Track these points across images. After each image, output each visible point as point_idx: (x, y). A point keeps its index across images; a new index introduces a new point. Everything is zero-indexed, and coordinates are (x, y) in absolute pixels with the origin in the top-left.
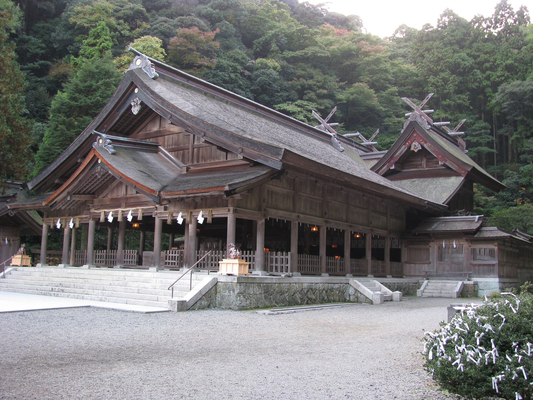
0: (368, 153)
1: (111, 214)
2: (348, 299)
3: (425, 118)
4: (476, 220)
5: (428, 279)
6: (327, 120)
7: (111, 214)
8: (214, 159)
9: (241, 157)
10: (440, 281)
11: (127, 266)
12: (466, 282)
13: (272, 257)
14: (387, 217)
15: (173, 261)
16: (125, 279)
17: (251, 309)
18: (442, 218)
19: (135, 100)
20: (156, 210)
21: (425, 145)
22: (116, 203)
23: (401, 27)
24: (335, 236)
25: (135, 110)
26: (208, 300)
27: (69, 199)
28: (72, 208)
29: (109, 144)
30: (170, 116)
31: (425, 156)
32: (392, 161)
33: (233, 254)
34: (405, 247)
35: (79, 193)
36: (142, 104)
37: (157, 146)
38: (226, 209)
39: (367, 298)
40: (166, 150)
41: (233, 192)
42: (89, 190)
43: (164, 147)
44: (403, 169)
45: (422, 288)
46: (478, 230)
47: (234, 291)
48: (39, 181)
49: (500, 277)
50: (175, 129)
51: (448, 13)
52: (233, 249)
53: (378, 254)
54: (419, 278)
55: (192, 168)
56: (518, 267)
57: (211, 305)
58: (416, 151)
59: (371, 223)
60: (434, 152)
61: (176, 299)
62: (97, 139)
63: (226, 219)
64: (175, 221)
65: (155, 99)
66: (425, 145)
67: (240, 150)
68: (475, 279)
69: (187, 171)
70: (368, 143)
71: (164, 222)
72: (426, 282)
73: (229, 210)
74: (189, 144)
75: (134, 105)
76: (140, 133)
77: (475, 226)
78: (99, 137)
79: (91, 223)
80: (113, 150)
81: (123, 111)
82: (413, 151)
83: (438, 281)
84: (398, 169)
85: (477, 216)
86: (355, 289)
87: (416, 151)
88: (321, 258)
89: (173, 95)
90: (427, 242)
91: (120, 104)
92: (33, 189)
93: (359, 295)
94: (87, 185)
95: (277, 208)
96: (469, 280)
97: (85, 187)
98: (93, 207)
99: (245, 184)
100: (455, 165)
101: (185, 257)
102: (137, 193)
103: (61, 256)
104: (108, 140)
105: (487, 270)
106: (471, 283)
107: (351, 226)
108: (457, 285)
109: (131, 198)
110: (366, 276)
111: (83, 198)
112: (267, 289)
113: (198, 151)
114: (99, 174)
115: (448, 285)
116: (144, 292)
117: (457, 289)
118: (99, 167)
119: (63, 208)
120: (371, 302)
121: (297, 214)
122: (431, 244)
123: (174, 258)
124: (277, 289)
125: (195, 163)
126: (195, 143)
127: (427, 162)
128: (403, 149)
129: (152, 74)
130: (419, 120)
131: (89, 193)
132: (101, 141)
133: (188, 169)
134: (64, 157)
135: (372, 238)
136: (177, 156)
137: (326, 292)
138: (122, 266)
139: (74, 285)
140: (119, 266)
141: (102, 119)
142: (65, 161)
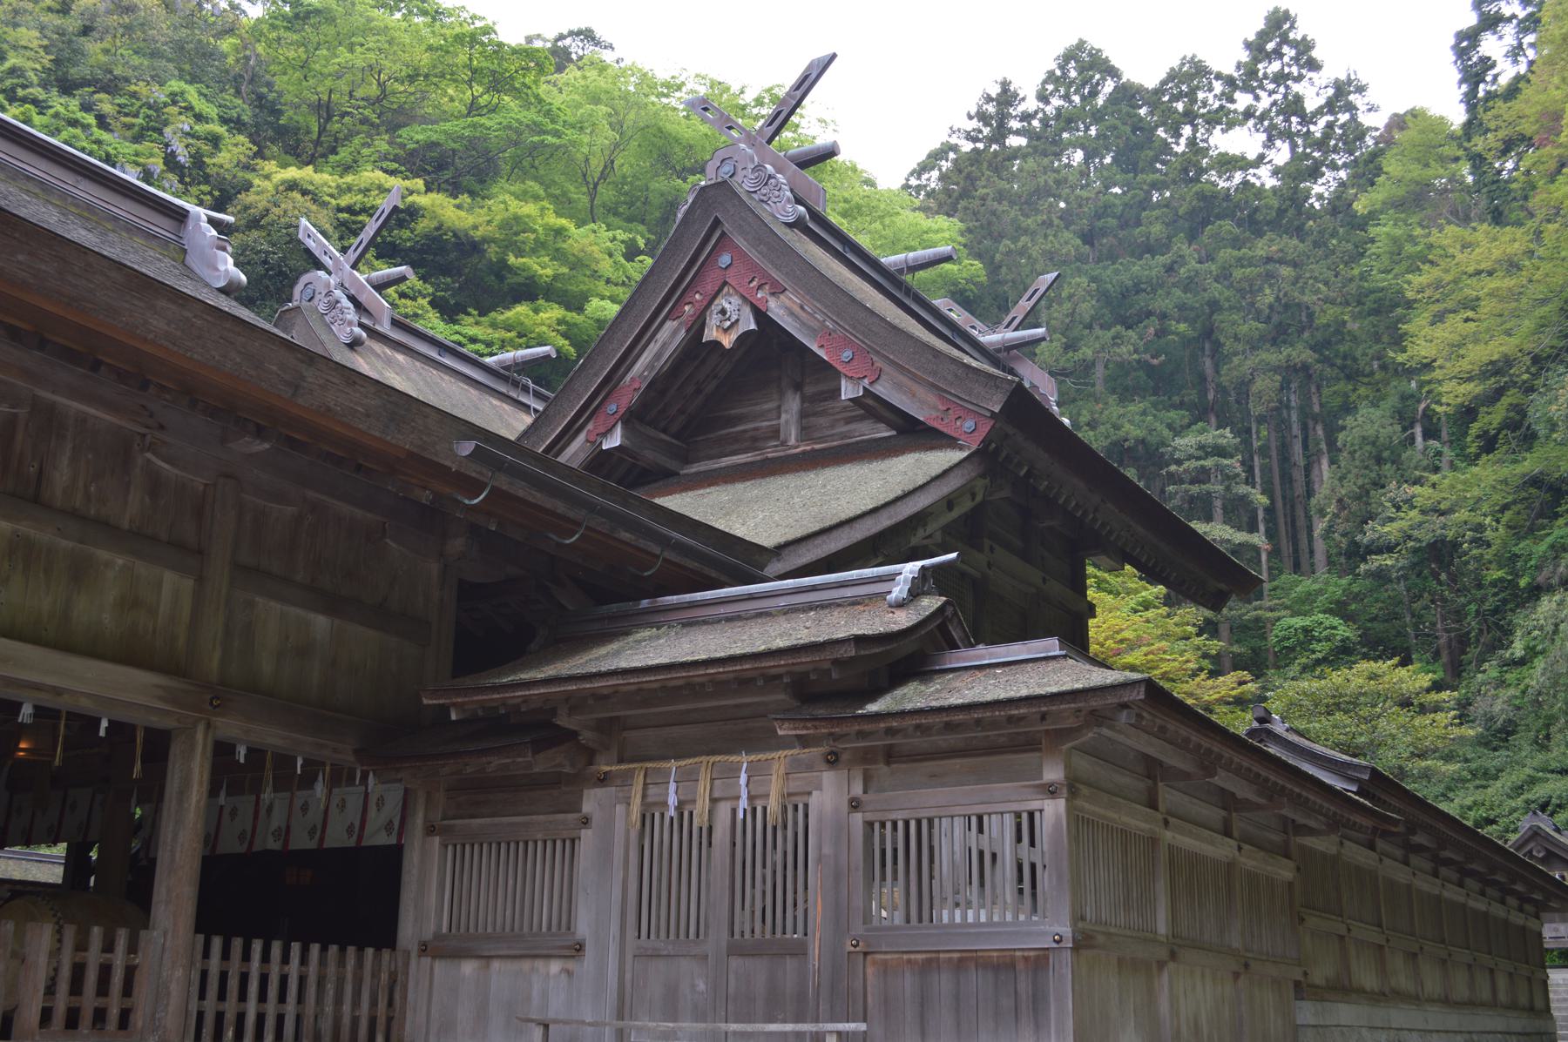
4: (898, 591)
14: (200, 580)
31: (798, 387)
32: (612, 408)
34: (430, 830)
44: (687, 461)
51: (1085, 64)
56: (1301, 990)
58: (727, 341)
60: (813, 332)
84: (651, 456)
85: (911, 569)
87: (727, 341)
90: (560, 792)
100: (921, 391)
122: (592, 801)
127: (803, 415)
128: (670, 336)
130: (744, 183)
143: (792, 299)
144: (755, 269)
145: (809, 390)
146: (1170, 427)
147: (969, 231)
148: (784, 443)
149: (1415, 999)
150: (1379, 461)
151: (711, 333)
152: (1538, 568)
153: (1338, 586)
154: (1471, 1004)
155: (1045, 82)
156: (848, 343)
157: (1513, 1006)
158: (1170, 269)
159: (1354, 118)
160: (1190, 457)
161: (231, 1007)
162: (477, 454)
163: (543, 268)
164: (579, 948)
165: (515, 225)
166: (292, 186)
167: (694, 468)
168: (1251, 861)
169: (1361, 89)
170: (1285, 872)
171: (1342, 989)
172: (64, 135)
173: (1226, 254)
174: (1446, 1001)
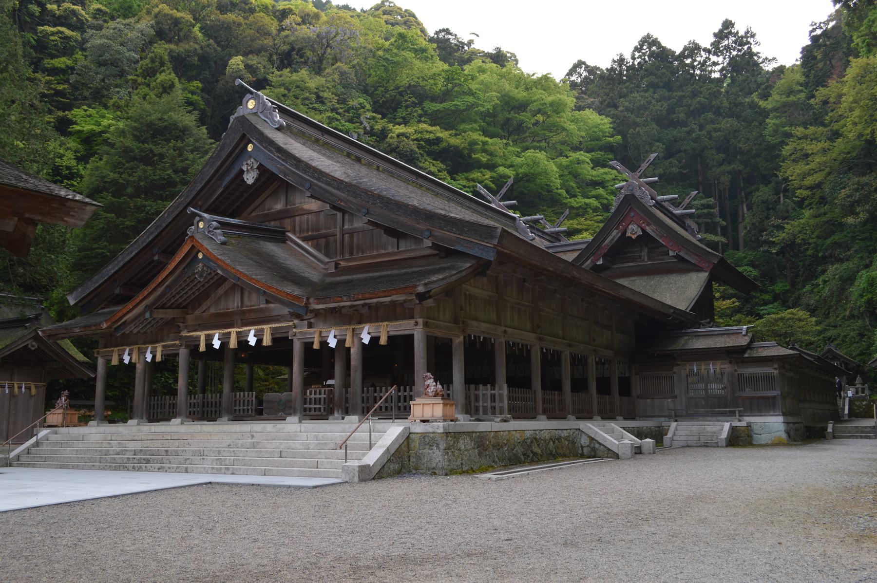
0: (555, 244)
1: (252, 333)
2: (580, 452)
3: (647, 191)
4: (744, 333)
5: (676, 421)
6: (499, 197)
7: (252, 333)
8: (377, 250)
9: (428, 243)
10: (698, 423)
11: (238, 417)
12: (736, 423)
13: (477, 392)
15: (318, 406)
16: (253, 436)
17: (463, 473)
18: (691, 330)
19: (249, 162)
20: (295, 328)
21: (647, 228)
22: (223, 321)
23: (580, 64)
24: (551, 361)
25: (250, 178)
26: (401, 463)
27: (147, 315)
28: (149, 331)
29: (215, 229)
30: (308, 185)
33: (432, 389)
34: (636, 374)
35: (163, 307)
36: (261, 168)
37: (284, 233)
38: (412, 322)
39: (609, 449)
40: (298, 238)
41: (427, 295)
42: (180, 301)
43: (294, 233)
45: (670, 435)
46: (749, 347)
47: (438, 447)
48: (88, 292)
49: (784, 414)
50: (313, 205)
51: (648, 41)
52: (430, 382)
53: (604, 387)
54: (663, 419)
55: (343, 264)
57: (403, 470)
58: (634, 237)
59: (594, 340)
61: (355, 463)
62: (195, 222)
63: (411, 337)
64: (324, 344)
65: (283, 160)
66: (647, 228)
67: (427, 233)
68: (748, 419)
69: (336, 268)
70: (553, 230)
71: (308, 346)
72: (674, 425)
73: (416, 324)
74: (335, 228)
75: (248, 170)
76: (254, 214)
77: (744, 341)
78: (197, 218)
79: (183, 352)
80: (223, 238)
81: (228, 179)
82: (630, 238)
83: (690, 423)
85: (745, 327)
86: (589, 437)
87: (634, 237)
88: (535, 393)
89: (314, 154)
91: (223, 169)
92: (76, 304)
93: (597, 446)
94: (178, 293)
95: (476, 319)
96: (740, 421)
97: (174, 297)
98: (186, 327)
99: (445, 282)
101: (336, 399)
102: (267, 302)
103: (91, 407)
104: (214, 223)
105: (763, 406)
106: (743, 424)
107: (570, 345)
108: (725, 428)
109: (251, 311)
110: (565, 418)
111: (169, 314)
112: (481, 441)
113: (351, 237)
114: (201, 276)
115: (709, 428)
116: (311, 455)
117: (724, 435)
118: (201, 265)
119: (135, 331)
120: (616, 456)
121: (504, 328)
123: (317, 401)
124: (493, 440)
125: (347, 256)
126: (346, 227)
127: (648, 252)
128: (615, 234)
129: (275, 122)
130: (637, 194)
131: (177, 307)
132: (201, 225)
133: (337, 265)
134: (131, 252)
135: (597, 363)
136: (317, 247)
137: (554, 442)
138: (231, 417)
139: (167, 451)
140: (225, 419)
141: (194, 193)
142: (132, 259)
147: (614, 122)
148: (643, 261)
150: (768, 209)
151: (628, 234)
152: (826, 250)
153: (751, 255)
155: (634, 51)
158: (688, 133)
159: (749, 48)
161: (155, 411)
163: (484, 158)
164: (676, 397)
165: (474, 143)
166: (403, 134)
169: (753, 36)
172: (334, 124)
173: (709, 127)
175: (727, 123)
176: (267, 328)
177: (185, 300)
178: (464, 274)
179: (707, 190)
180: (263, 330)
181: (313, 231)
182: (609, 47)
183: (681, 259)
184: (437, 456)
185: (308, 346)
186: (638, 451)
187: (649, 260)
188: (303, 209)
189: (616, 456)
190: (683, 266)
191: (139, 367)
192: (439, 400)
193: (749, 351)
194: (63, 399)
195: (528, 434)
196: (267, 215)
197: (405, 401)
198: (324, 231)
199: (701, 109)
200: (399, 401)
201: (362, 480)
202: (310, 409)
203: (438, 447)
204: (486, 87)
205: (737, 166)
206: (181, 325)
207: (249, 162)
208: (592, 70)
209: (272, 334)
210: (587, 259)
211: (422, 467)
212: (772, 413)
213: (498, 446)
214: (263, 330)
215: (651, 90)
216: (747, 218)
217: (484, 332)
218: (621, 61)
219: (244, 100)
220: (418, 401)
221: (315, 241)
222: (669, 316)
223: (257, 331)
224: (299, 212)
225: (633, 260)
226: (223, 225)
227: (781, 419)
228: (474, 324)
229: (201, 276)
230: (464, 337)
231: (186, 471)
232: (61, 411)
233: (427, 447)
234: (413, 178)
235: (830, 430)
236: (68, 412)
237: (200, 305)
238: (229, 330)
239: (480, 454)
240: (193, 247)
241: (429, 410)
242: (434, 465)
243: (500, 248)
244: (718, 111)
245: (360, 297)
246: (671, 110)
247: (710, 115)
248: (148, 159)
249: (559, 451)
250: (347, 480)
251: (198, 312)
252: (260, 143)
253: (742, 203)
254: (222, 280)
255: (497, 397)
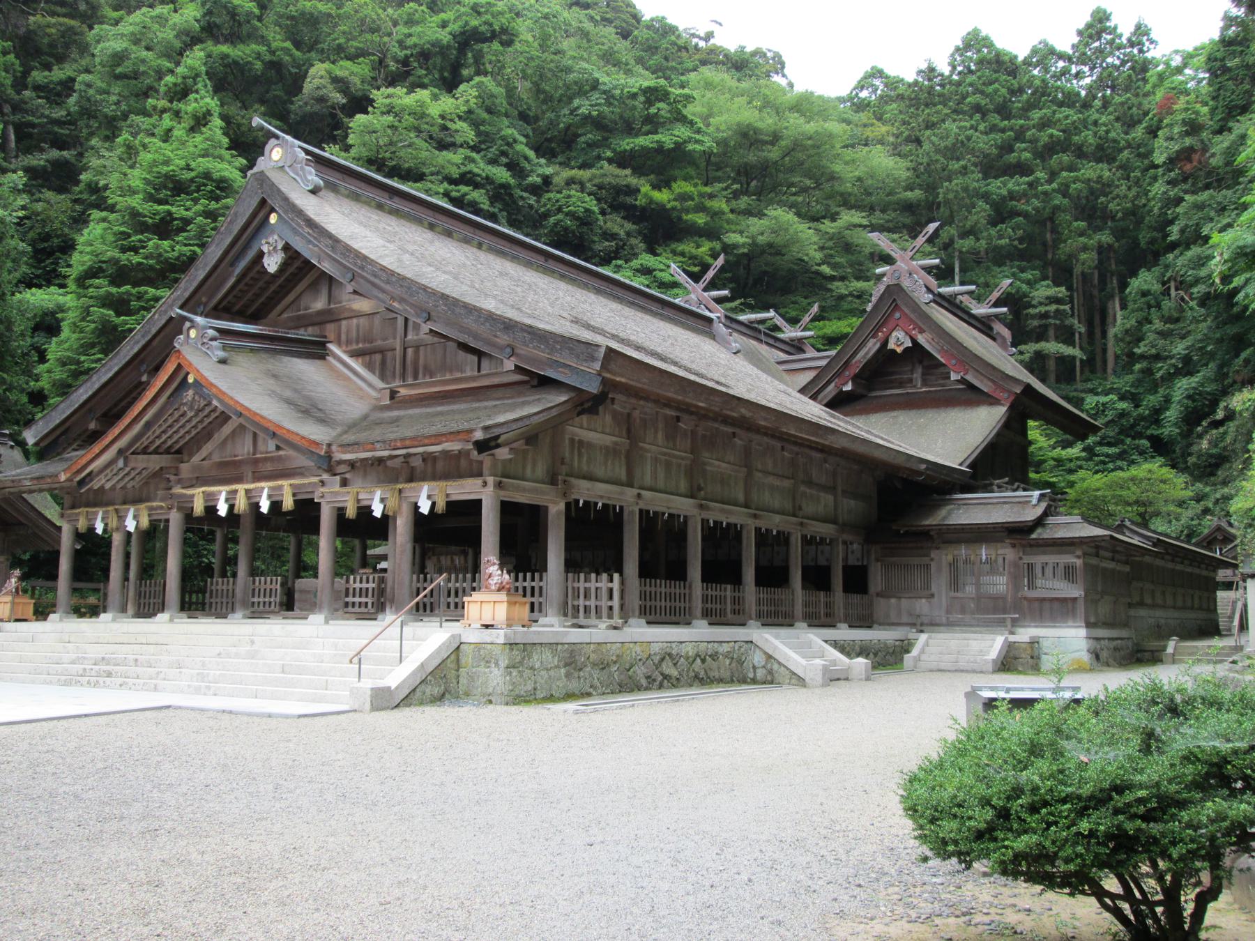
1: (223, 497)
2: (751, 675)
3: (923, 278)
4: (1034, 501)
6: (702, 285)
9: (509, 365)
11: (257, 613)
12: (1012, 638)
15: (363, 600)
16: (253, 642)
19: (271, 240)
22: (229, 472)
25: (272, 264)
26: (441, 684)
27: (121, 463)
28: (129, 486)
31: (921, 362)
34: (877, 560)
35: (145, 451)
36: (287, 248)
37: (323, 345)
38: (479, 481)
40: (345, 352)
41: (493, 444)
43: (339, 344)
44: (870, 390)
45: (915, 652)
46: (1039, 522)
47: (497, 664)
48: (52, 426)
49: (1089, 625)
51: (974, 41)
55: (403, 392)
56: (1130, 605)
58: (899, 350)
59: (800, 508)
60: (939, 352)
63: (478, 503)
74: (395, 338)
75: (269, 252)
76: (285, 315)
77: (1031, 515)
78: (188, 324)
81: (243, 264)
82: (894, 351)
86: (766, 653)
87: (899, 350)
93: (776, 667)
95: (590, 478)
97: (158, 437)
98: (179, 481)
100: (985, 381)
107: (755, 516)
109: (266, 459)
111: (155, 462)
112: (572, 659)
116: (298, 672)
119: (108, 486)
125: (410, 381)
126: (409, 337)
127: (923, 374)
128: (872, 346)
130: (906, 283)
131: (167, 452)
132: (193, 333)
133: (393, 394)
136: (370, 367)
137: (703, 661)
138: (248, 613)
139: (136, 660)
143: (927, 335)
144: (912, 321)
145: (926, 363)
146: (1028, 283)
149: (1164, 607)
151: (891, 346)
154: (1184, 608)
156: (953, 356)
157: (1200, 608)
158: (1030, 185)
160: (1041, 304)
162: (927, 469)
163: (700, 219)
165: (683, 197)
167: (874, 394)
168: (1120, 567)
170: (1127, 569)
171: (1141, 604)
174: (1174, 607)
175: (1091, 171)
176: (285, 483)
177: (176, 442)
178: (554, 412)
179: (1062, 274)
180: (236, 491)
181: (364, 341)
182: (920, 48)
183: (971, 387)
184: (496, 678)
185: (341, 512)
186: (834, 678)
187: (925, 383)
188: (352, 310)
189: (801, 682)
190: (971, 396)
191: (117, 539)
192: (503, 596)
193: (1039, 530)
194: (13, 580)
195: (656, 648)
196: (304, 316)
197: (457, 595)
198: (379, 343)
199: (1052, 148)
200: (449, 595)
201: (375, 708)
202: (354, 603)
203: (497, 664)
204: (716, 111)
205: (1105, 237)
206: (172, 478)
207: (271, 240)
208: (892, 83)
209: (294, 495)
210: (828, 383)
211: (475, 692)
212: (1070, 624)
213: (603, 666)
214: (280, 488)
215: (978, 116)
216: (1121, 321)
217: (601, 497)
218: (931, 71)
219: (267, 148)
220: (476, 596)
221: (367, 358)
222: (919, 473)
223: (229, 493)
224: (346, 315)
225: (901, 384)
226: (223, 332)
227: (1082, 632)
228: (584, 484)
229: (191, 408)
230: (568, 505)
231: (156, 689)
232: (9, 599)
233: (483, 663)
234: (540, 260)
235: (1170, 650)
236: (18, 600)
237: (199, 449)
238: (280, 482)
239: (568, 675)
240: (179, 367)
241: (489, 608)
242: (491, 690)
243: (608, 375)
244: (1080, 153)
245: (399, 444)
246: (1007, 148)
247: (1065, 158)
248: (165, 228)
249: (711, 674)
250: (356, 707)
251: (196, 459)
252: (286, 212)
253: (1112, 297)
254: (224, 418)
255: (593, 591)
